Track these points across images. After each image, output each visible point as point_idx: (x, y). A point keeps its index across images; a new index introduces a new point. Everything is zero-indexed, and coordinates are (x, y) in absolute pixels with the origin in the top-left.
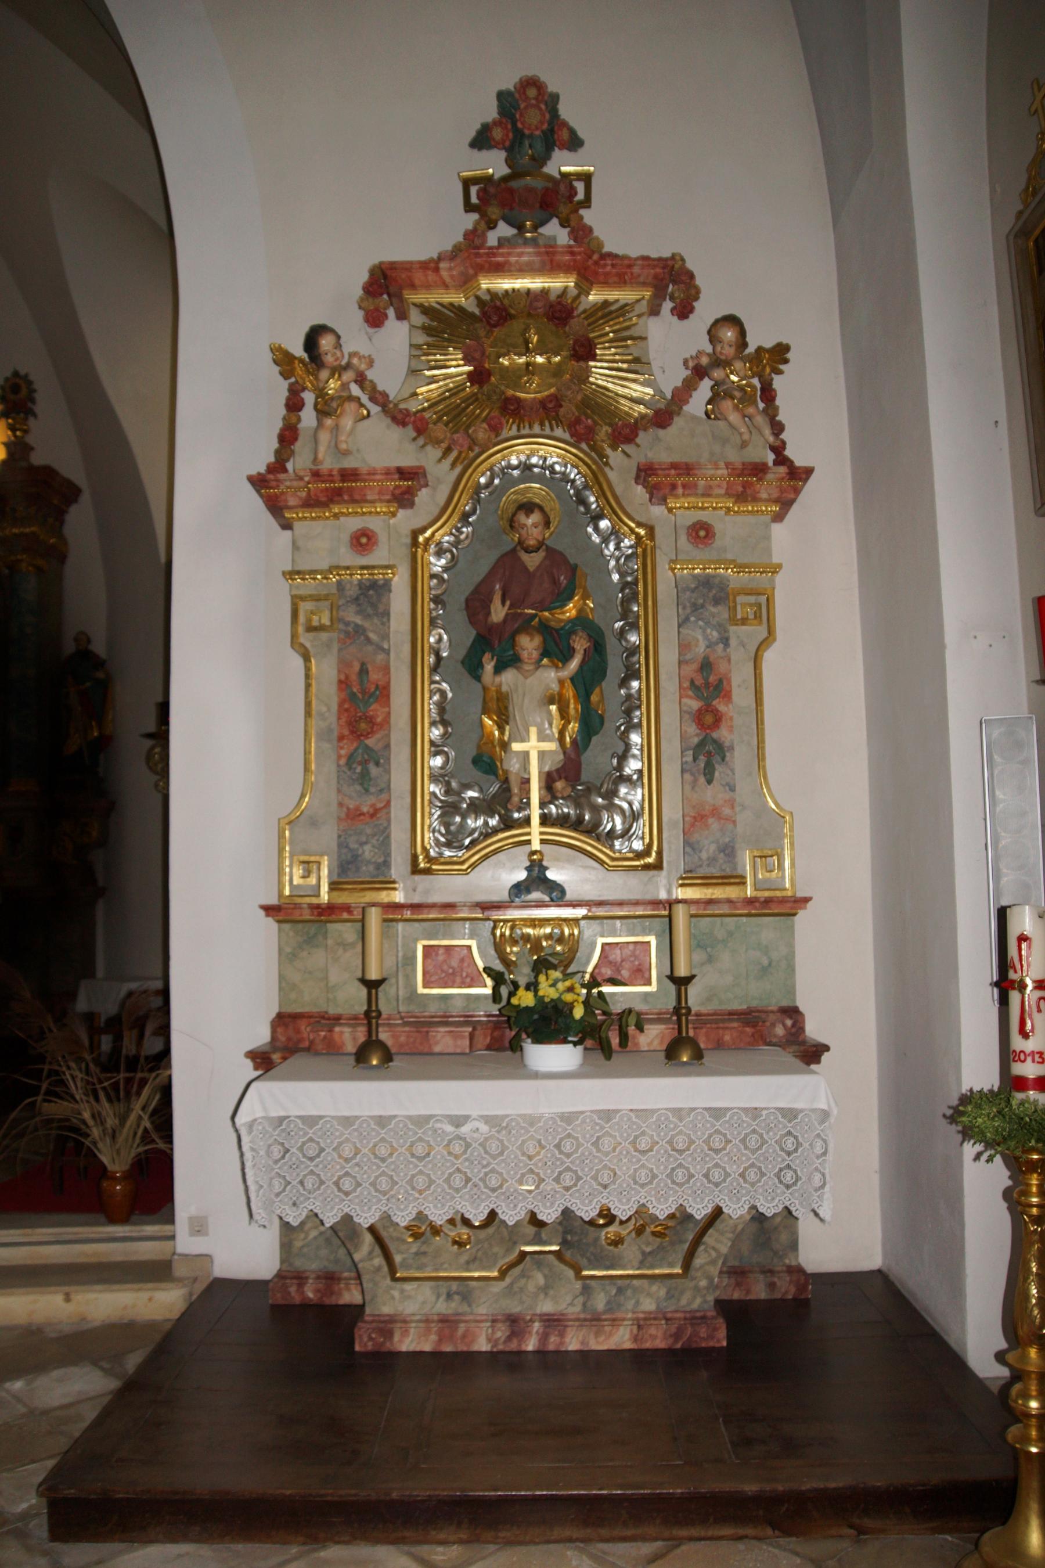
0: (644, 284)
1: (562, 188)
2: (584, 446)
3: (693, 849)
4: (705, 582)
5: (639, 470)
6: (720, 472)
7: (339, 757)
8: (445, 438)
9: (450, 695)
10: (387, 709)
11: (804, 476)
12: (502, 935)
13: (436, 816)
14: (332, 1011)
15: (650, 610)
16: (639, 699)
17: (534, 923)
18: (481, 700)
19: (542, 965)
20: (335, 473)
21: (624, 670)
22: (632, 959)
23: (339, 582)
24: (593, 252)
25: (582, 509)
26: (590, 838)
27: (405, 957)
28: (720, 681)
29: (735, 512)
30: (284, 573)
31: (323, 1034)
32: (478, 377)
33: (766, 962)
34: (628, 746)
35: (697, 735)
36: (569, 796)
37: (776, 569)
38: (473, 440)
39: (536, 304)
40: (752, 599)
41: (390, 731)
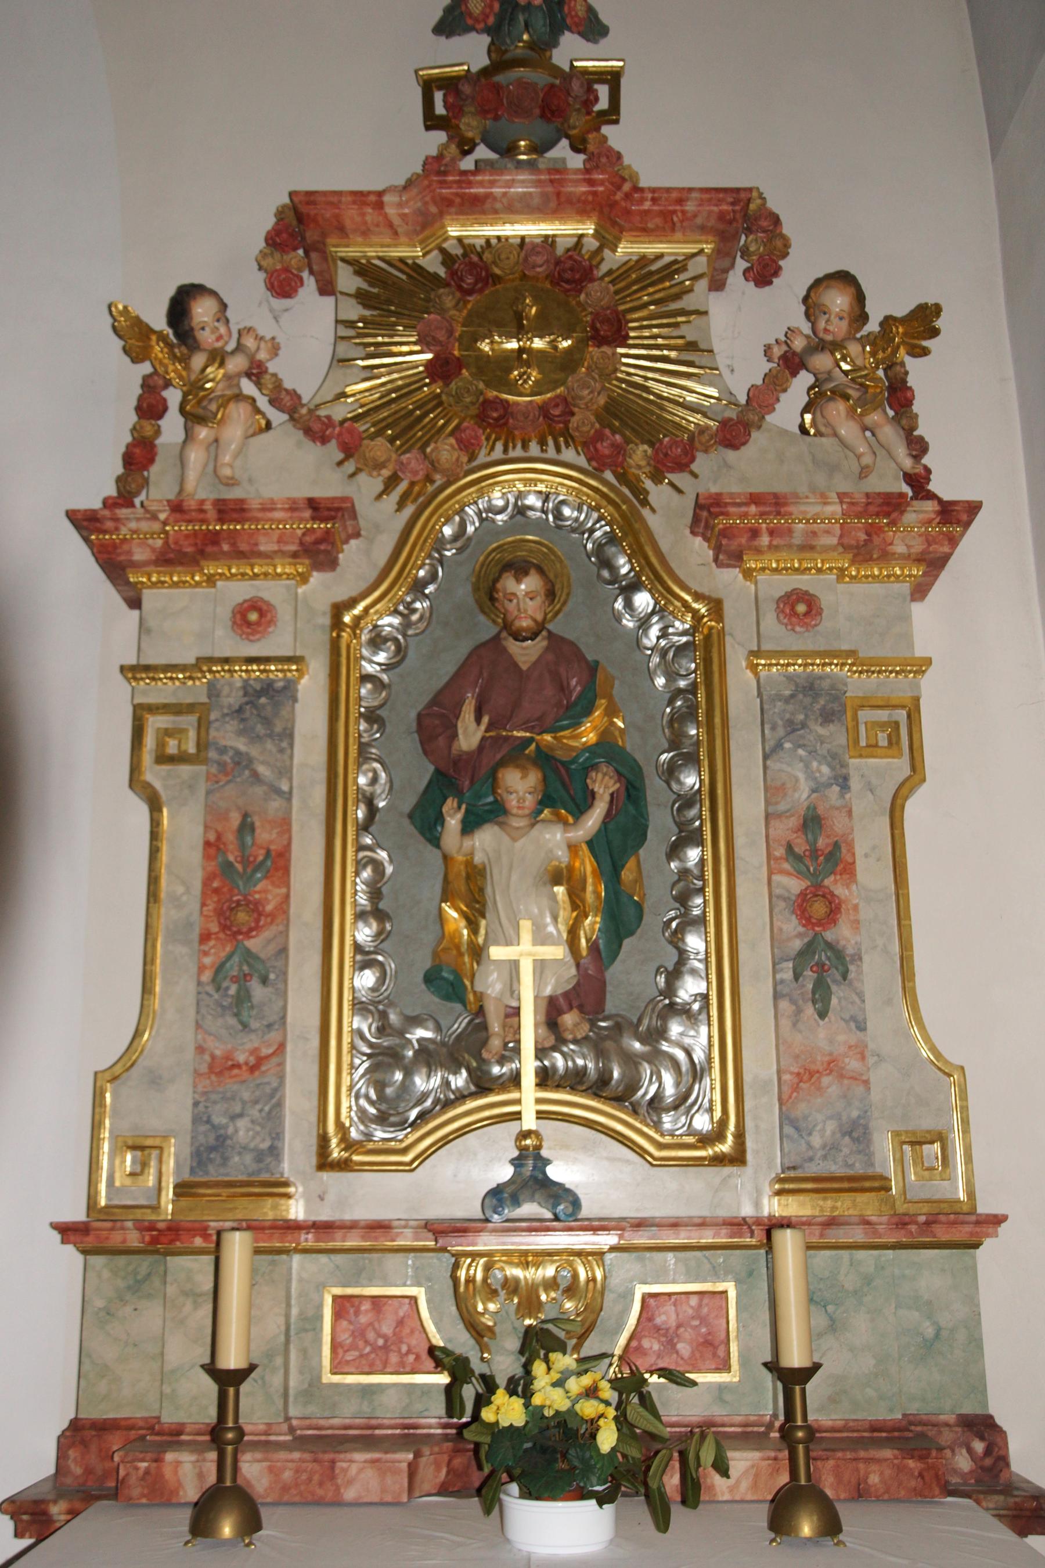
0: (703, 229)
1: (576, 86)
2: (608, 475)
3: (797, 1129)
4: (809, 687)
5: (698, 506)
6: (829, 509)
7: (201, 969)
8: (389, 460)
9: (389, 869)
10: (284, 890)
11: (964, 517)
12: (470, 1280)
13: (361, 1070)
14: (169, 1417)
15: (718, 732)
16: (702, 877)
17: (526, 1258)
18: (441, 877)
19: (538, 1343)
20: (208, 506)
21: (676, 830)
22: (696, 1323)
23: (211, 685)
24: (624, 180)
25: (606, 574)
26: (622, 1109)
27: (303, 1317)
28: (836, 845)
29: (852, 577)
30: (122, 669)
31: (145, 1464)
32: (441, 369)
33: (930, 1332)
34: (683, 956)
35: (800, 935)
36: (586, 1038)
37: (923, 665)
38: (432, 463)
39: (533, 259)
40: (883, 715)
41: (287, 926)
